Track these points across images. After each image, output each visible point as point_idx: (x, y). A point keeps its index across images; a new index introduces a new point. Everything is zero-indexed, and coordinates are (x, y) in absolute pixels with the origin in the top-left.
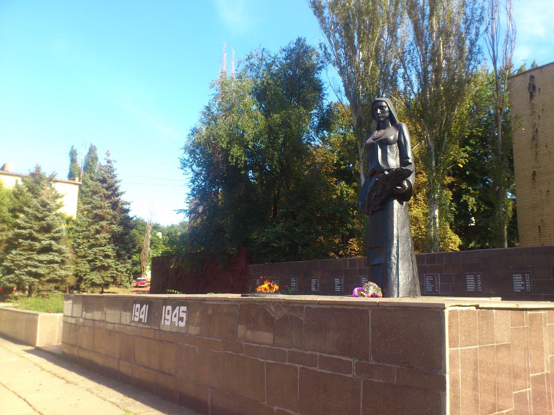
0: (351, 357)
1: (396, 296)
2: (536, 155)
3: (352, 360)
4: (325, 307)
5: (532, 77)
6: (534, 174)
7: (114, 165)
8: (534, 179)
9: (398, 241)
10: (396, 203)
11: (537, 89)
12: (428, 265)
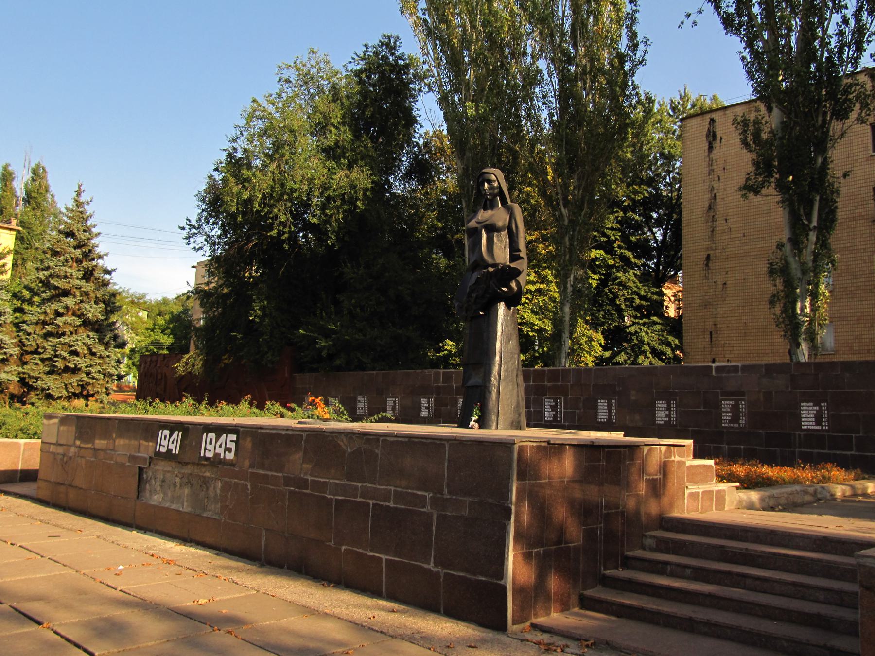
0: (426, 491)
1: (494, 427)
2: (712, 231)
3: (426, 494)
4: (403, 440)
5: (712, 121)
6: (708, 257)
7: (89, 209)
8: (707, 265)
9: (501, 358)
10: (501, 307)
11: (718, 138)
12: (549, 384)
